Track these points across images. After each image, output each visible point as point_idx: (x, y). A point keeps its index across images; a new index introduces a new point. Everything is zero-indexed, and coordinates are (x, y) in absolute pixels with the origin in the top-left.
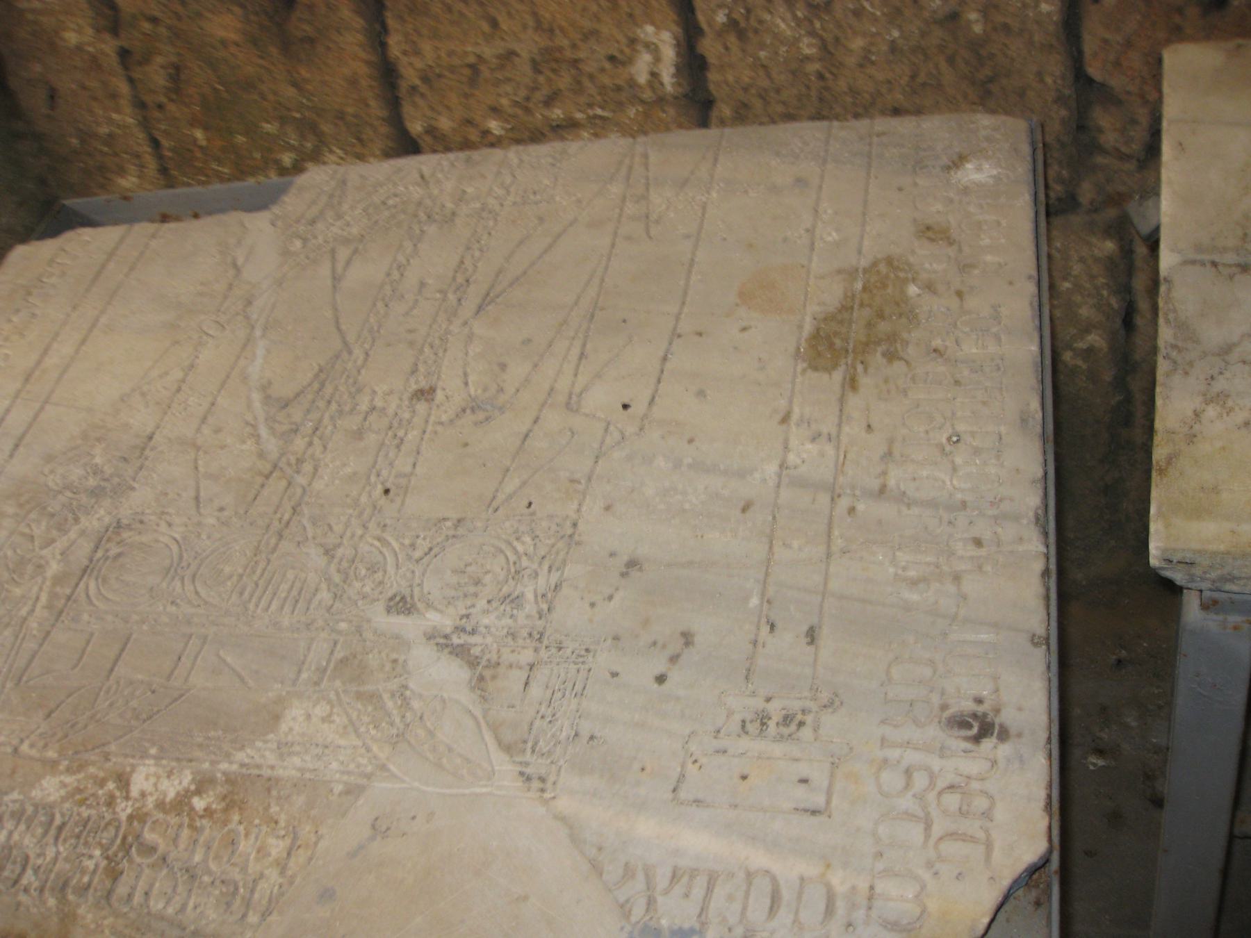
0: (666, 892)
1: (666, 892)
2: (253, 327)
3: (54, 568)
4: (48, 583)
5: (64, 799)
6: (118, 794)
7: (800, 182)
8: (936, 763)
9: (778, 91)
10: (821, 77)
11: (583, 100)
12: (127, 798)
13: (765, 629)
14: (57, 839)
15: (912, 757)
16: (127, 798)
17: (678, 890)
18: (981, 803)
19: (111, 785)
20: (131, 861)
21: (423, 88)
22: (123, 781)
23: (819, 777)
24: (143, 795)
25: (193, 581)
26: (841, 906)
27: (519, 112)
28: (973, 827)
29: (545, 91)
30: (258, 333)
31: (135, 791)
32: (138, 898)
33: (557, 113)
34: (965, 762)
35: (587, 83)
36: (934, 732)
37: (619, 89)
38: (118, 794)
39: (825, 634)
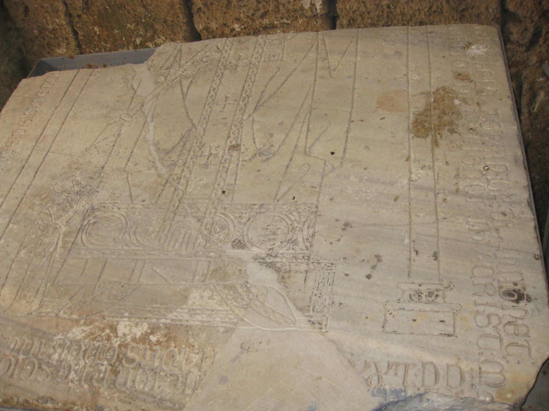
0: (386, 373)
1: (386, 373)
2: (146, 117)
3: (64, 229)
4: (61, 236)
5: (85, 338)
6: (112, 335)
7: (398, 53)
8: (501, 313)
9: (369, 13)
10: (388, 7)
11: (279, 16)
13: (413, 254)
14: (84, 357)
17: (392, 372)
18: (523, 330)
19: (108, 331)
20: (123, 366)
21: (203, 9)
22: (114, 329)
23: (448, 319)
24: (125, 335)
26: (467, 377)
27: (249, 20)
28: (521, 340)
29: (262, 11)
30: (149, 119)
31: (120, 334)
32: (129, 384)
33: (266, 21)
34: (514, 312)
35: (281, 8)
36: (497, 299)
37: (296, 10)
38: (112, 335)
39: (441, 254)
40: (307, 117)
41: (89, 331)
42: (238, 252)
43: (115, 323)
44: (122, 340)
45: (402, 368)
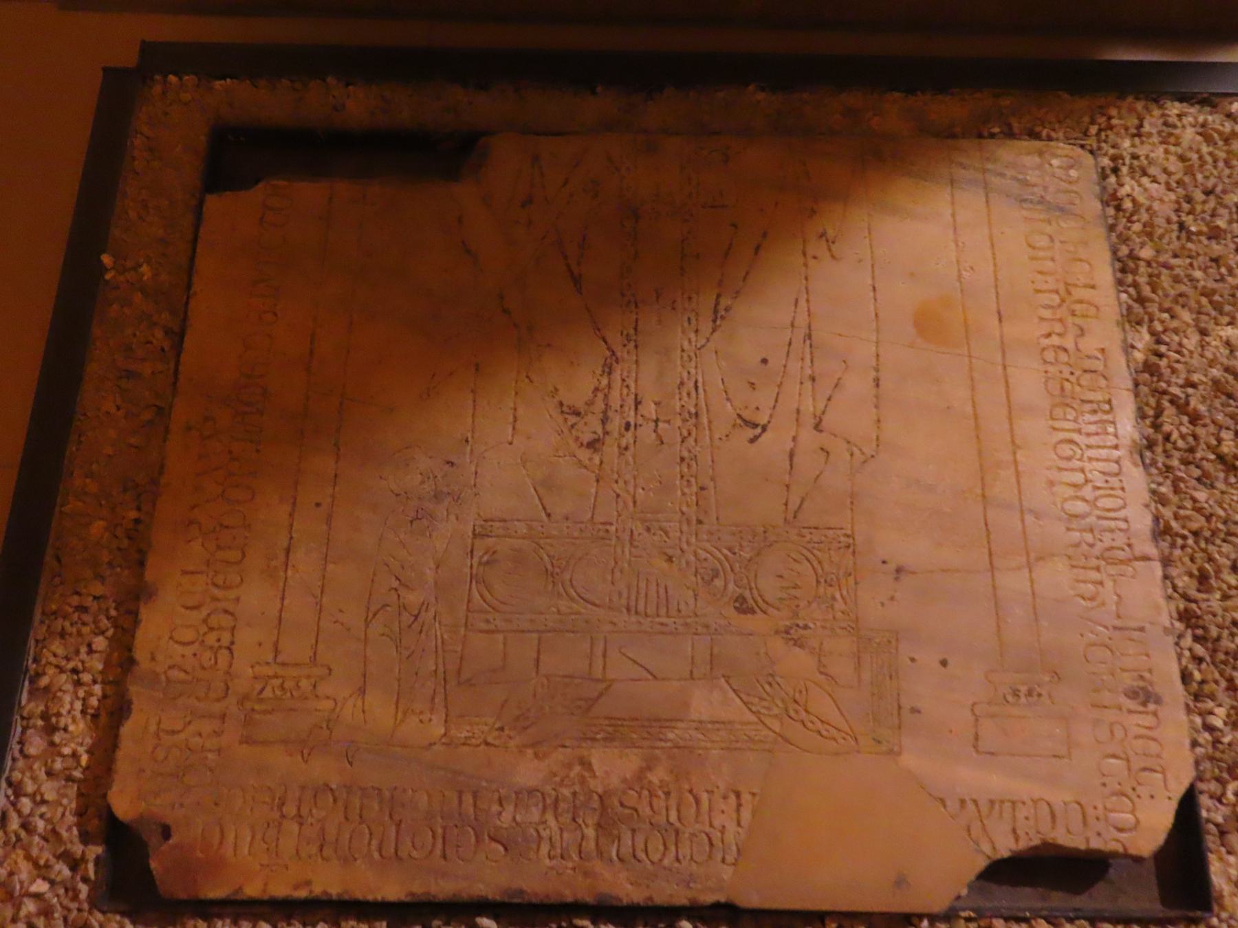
6: (587, 774)
19: (577, 769)
22: (586, 764)
38: (587, 774)
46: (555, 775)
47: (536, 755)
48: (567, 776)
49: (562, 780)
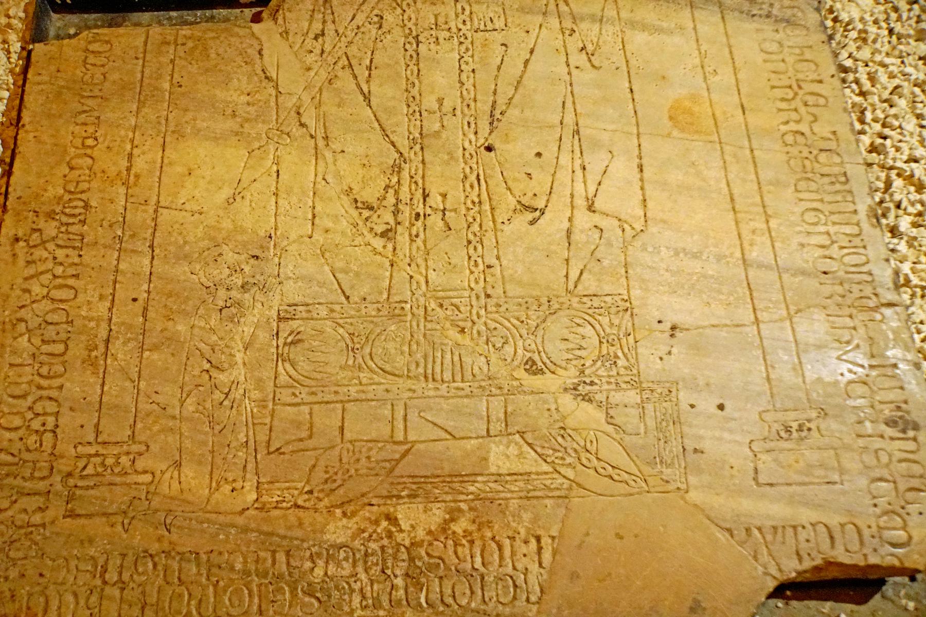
6: (394, 529)
12: (401, 531)
15: (878, 443)
16: (401, 531)
19: (384, 524)
22: (392, 519)
25: (372, 359)
31: (405, 525)
38: (394, 529)
40: (576, 142)
41: (355, 526)
42: (536, 382)
43: (392, 510)
44: (412, 535)
45: (790, 531)
46: (363, 531)
47: (344, 514)
48: (375, 531)
49: (371, 536)
